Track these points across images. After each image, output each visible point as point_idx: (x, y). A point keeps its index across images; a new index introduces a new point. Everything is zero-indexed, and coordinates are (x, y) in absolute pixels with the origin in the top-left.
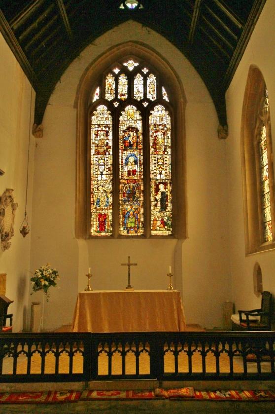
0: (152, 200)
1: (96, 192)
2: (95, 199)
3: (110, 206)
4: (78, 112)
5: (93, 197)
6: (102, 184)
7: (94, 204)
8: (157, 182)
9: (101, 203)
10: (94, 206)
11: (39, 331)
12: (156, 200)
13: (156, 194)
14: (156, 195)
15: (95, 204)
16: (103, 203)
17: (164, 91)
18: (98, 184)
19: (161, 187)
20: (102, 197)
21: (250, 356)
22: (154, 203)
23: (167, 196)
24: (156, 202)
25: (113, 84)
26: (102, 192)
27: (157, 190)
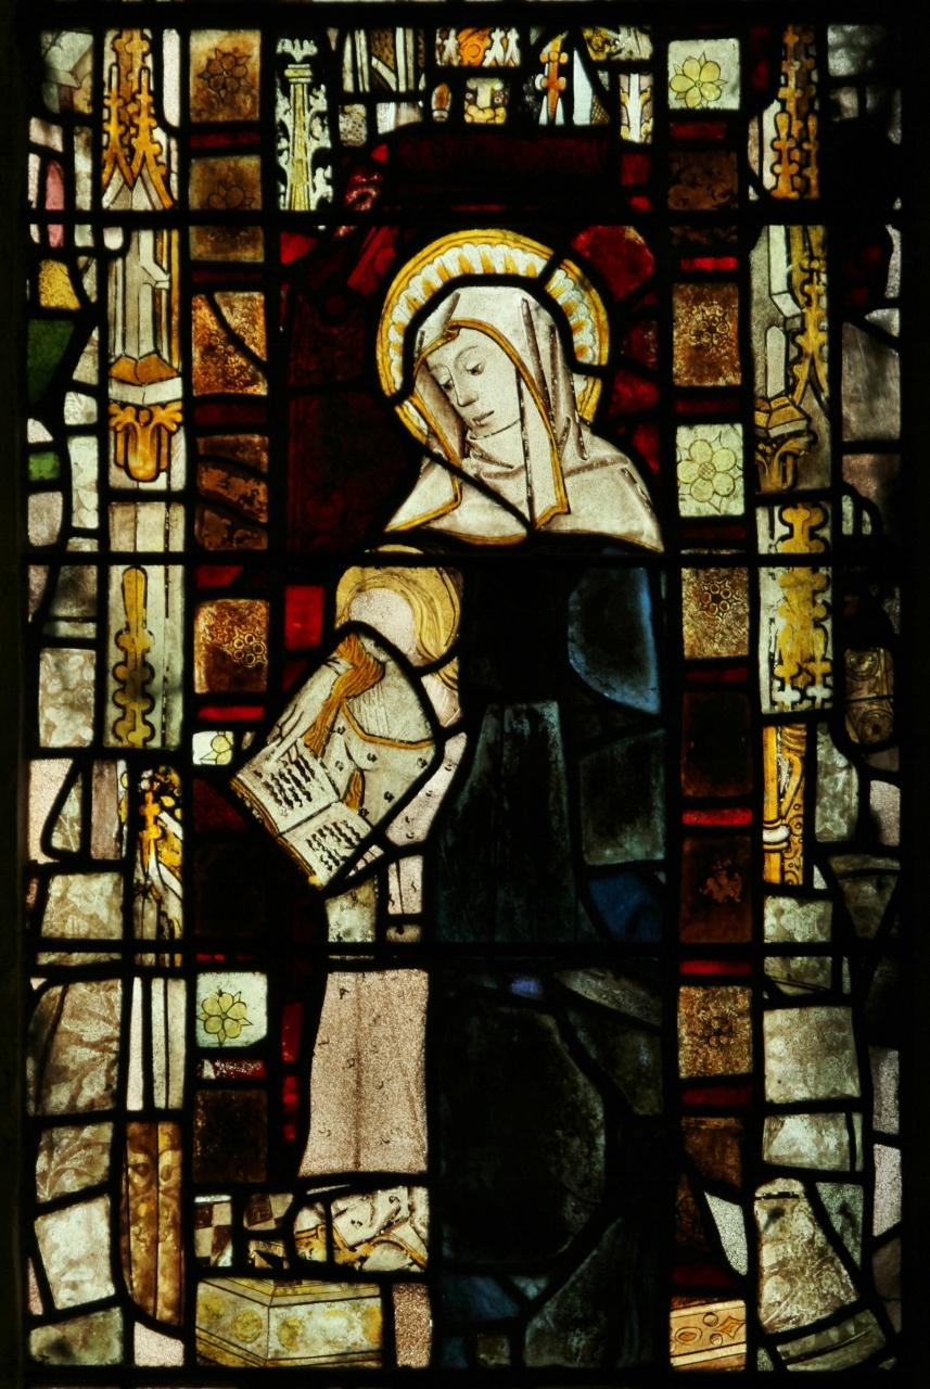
0: (82, 906)
4: (302, 1299)
8: (303, 131)
12: (250, 901)
13: (245, 632)
14: (249, 700)
19: (488, 351)
21: (88, 546)
22: (126, 1040)
23: (847, 1071)
24: (242, 1001)
27: (309, 469)
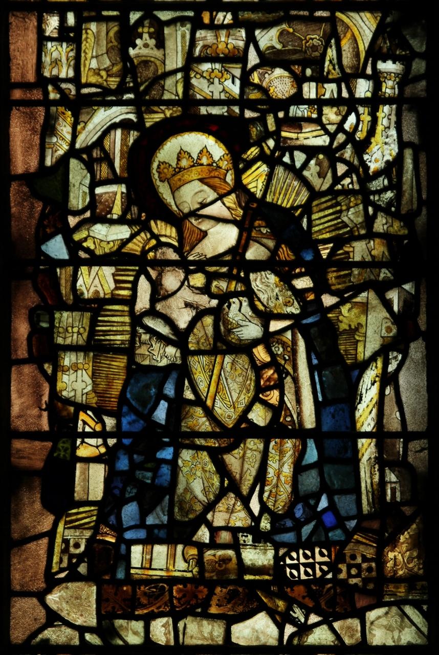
1: (108, 235)
2: (76, 382)
3: (384, 522)
5: (46, 351)
6: (217, 86)
7: (60, 499)
9: (196, 476)
10: (74, 536)
11: (254, 407)
15: (93, 481)
16: (244, 460)
17: (313, 357)
18: (135, 83)
20: (224, 344)
25: (249, 480)
26: (222, 238)
